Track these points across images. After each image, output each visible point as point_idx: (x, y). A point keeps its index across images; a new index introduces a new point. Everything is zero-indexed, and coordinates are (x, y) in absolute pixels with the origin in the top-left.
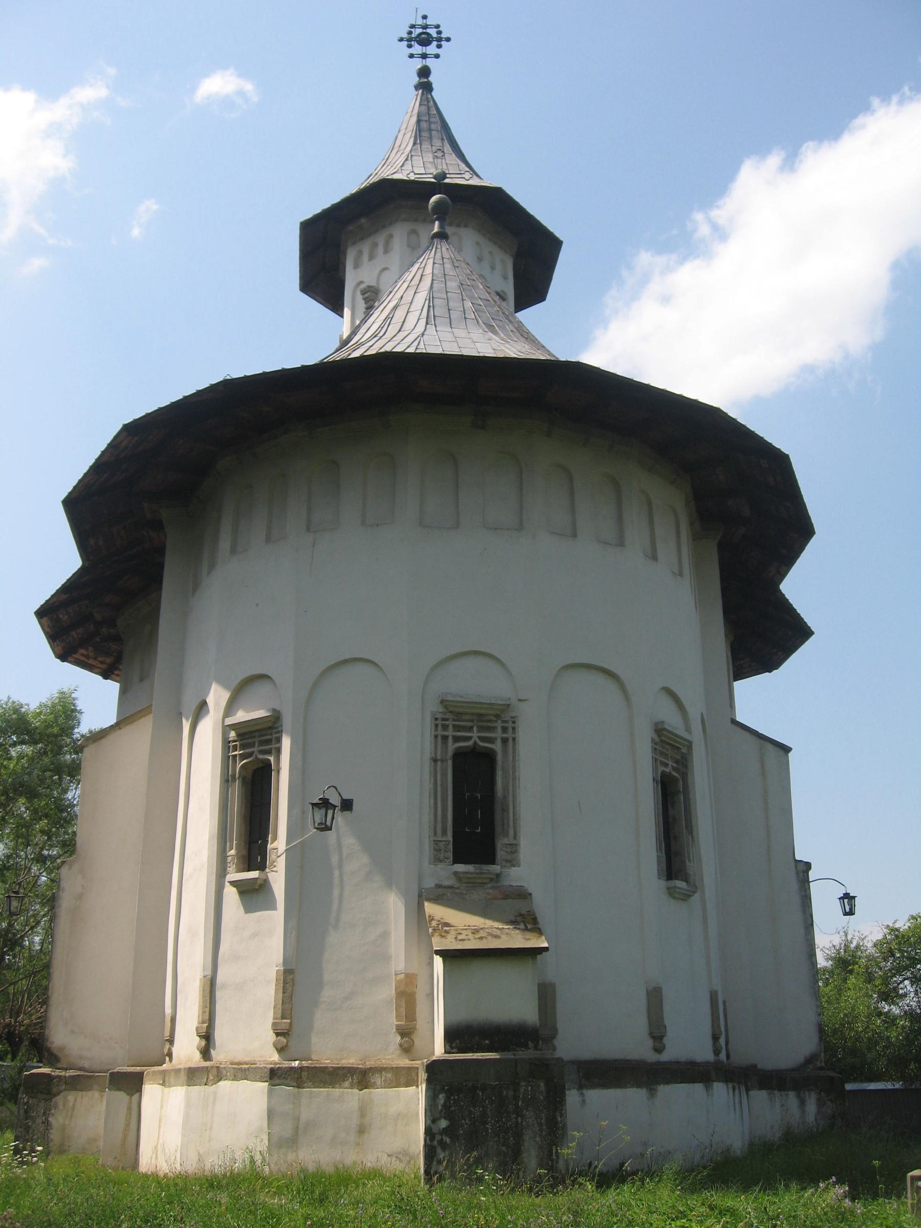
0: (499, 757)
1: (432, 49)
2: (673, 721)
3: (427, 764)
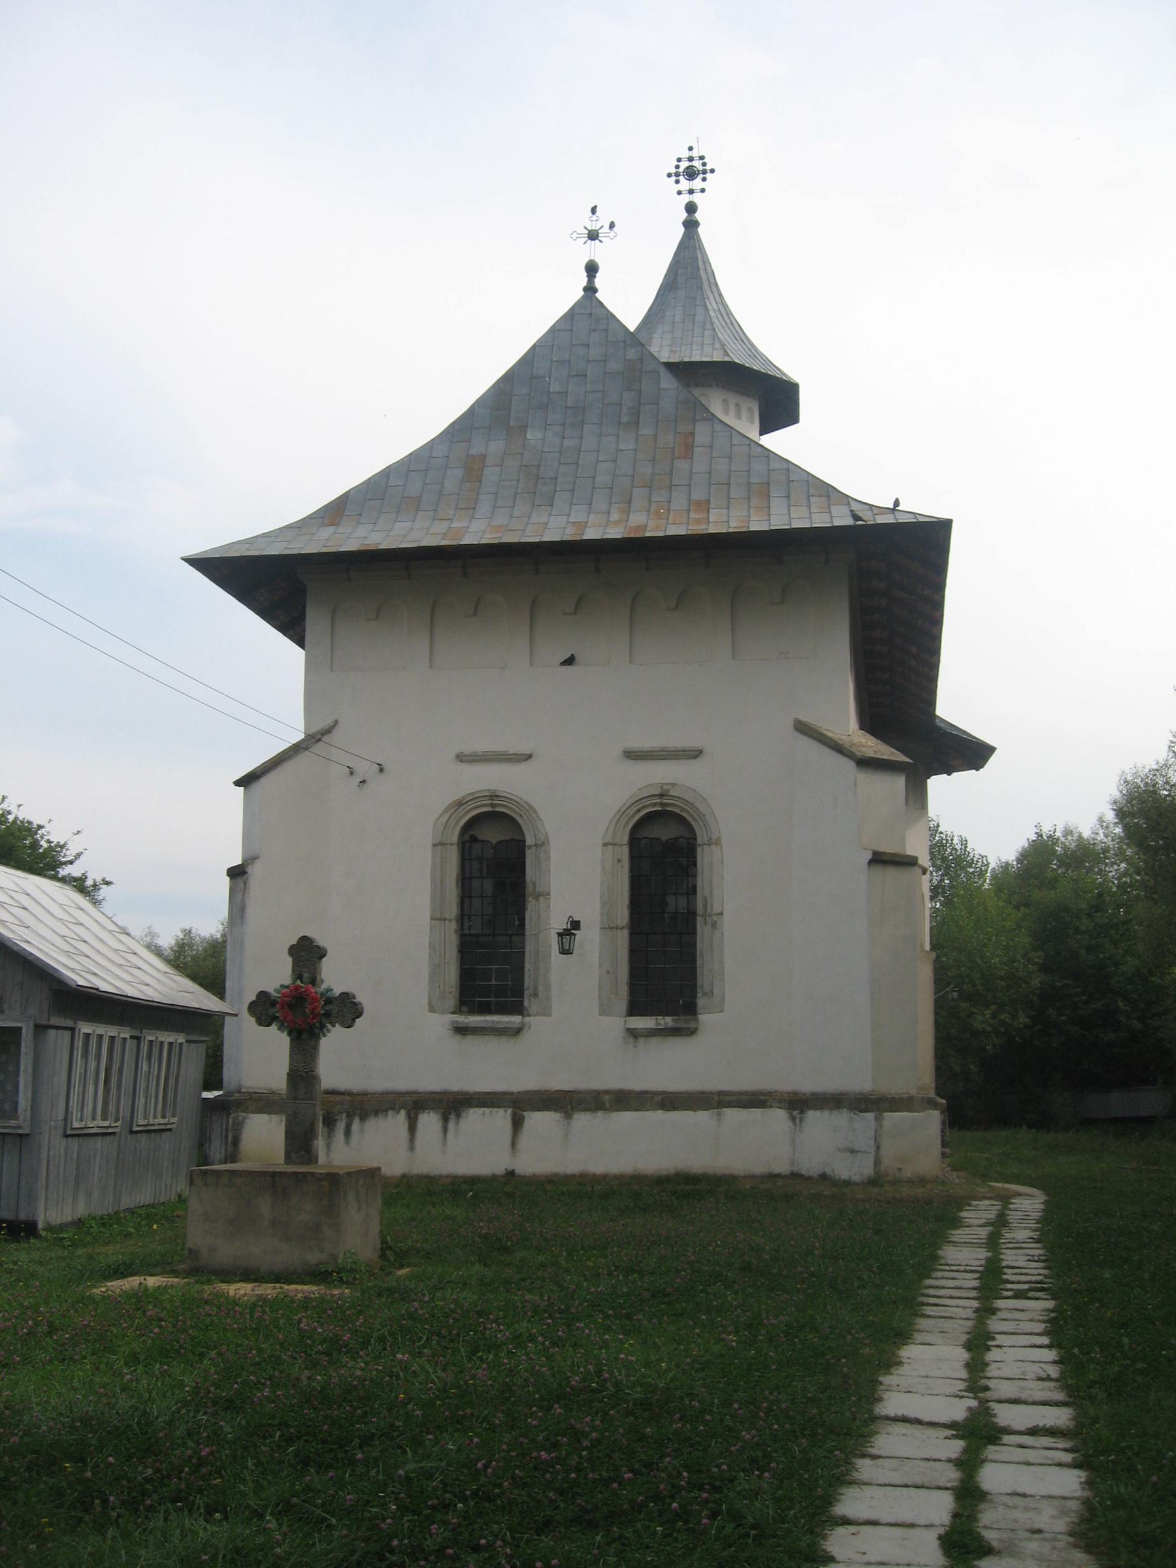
1: (697, 183)
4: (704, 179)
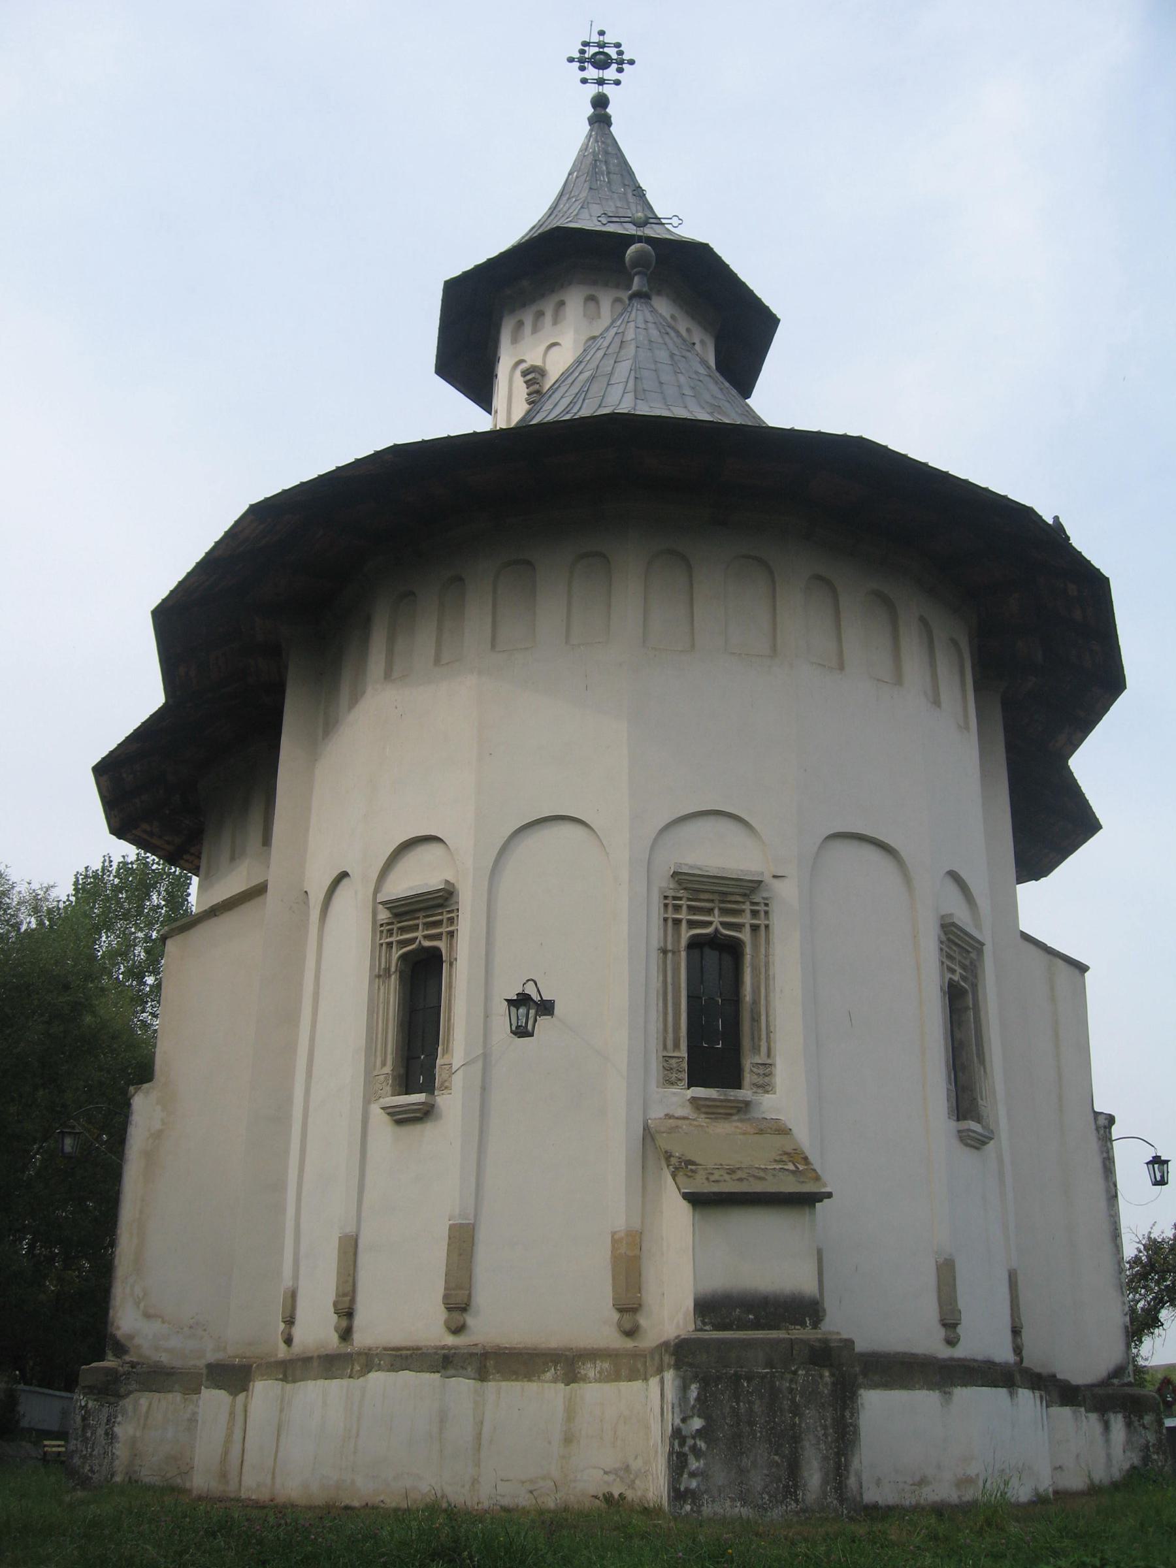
0: (748, 950)
1: (610, 73)
2: (962, 916)
3: (655, 956)
4: (620, 70)
